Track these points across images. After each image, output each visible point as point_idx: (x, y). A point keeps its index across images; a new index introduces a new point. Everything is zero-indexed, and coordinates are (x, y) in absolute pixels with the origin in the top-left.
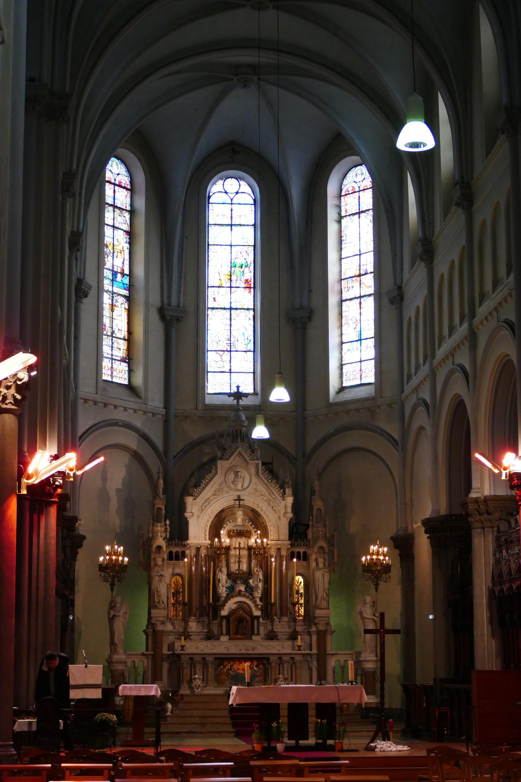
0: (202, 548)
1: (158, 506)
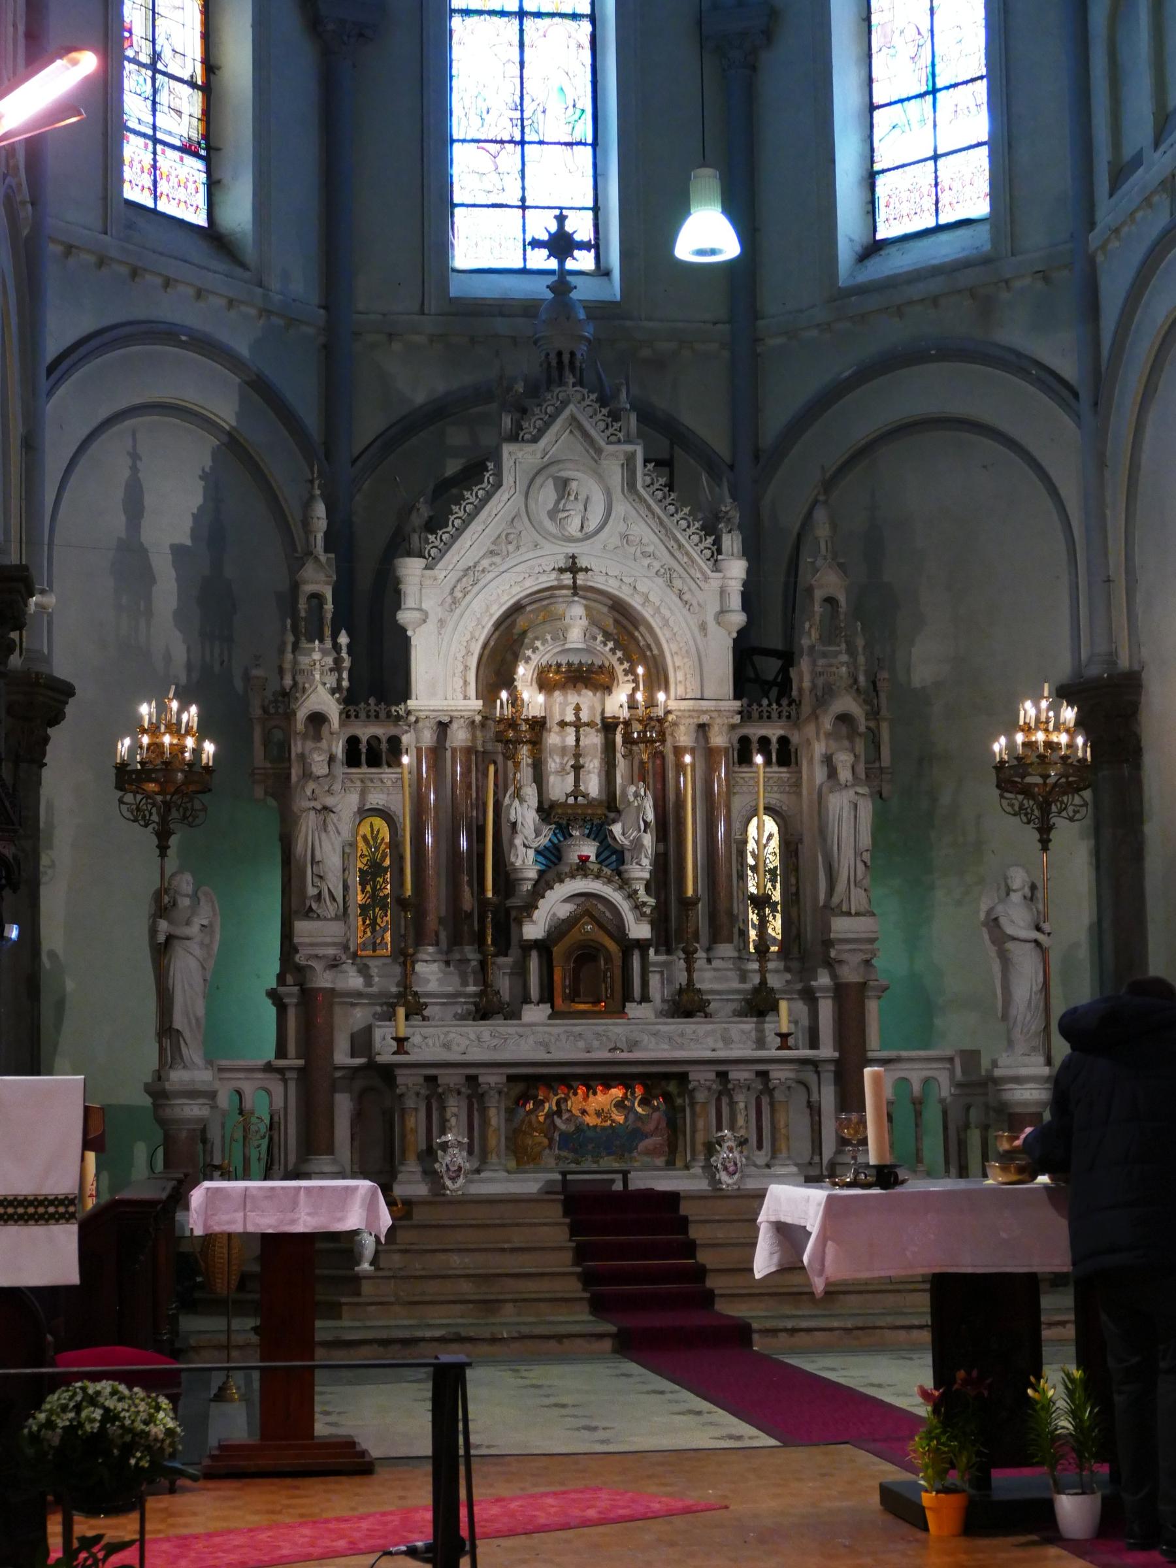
0: (455, 726)
1: (309, 588)
